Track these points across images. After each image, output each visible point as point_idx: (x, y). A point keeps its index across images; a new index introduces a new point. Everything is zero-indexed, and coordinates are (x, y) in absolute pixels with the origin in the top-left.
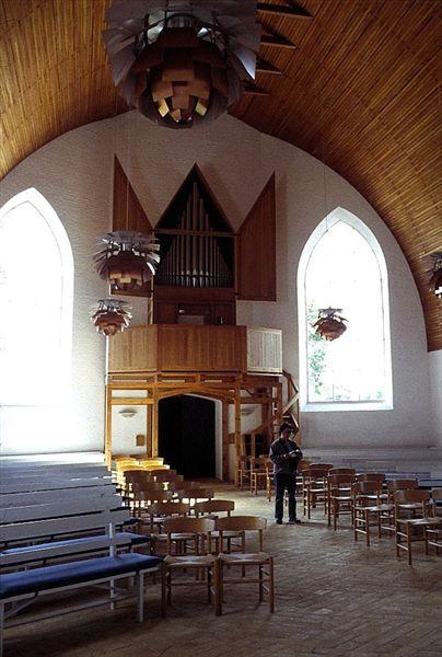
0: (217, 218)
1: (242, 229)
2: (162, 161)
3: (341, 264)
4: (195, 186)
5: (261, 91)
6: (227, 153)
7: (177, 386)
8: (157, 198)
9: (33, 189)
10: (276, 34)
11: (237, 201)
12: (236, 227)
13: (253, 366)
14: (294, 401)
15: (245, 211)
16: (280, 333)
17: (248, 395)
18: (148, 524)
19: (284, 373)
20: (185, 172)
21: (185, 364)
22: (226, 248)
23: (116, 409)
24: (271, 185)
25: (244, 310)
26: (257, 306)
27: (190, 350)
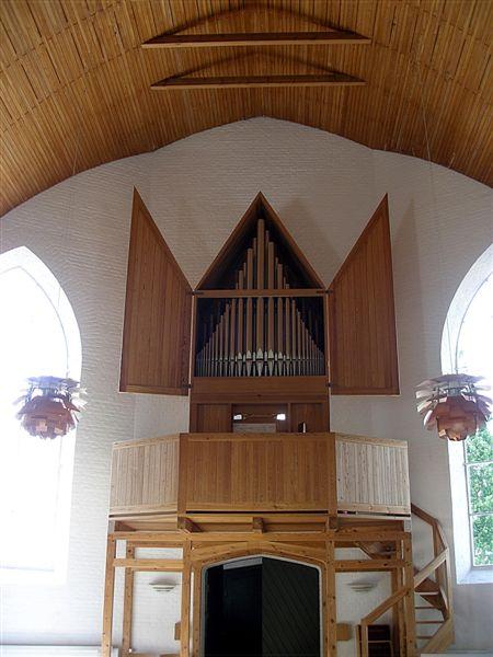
0: (295, 269)
1: (336, 283)
2: (213, 183)
3: (236, 418)
4: (259, 223)
5: (353, 78)
6: (312, 180)
7: (239, 545)
8: (197, 250)
9: (24, 247)
10: (336, 72)
11: (327, 245)
12: (327, 285)
13: (347, 497)
14: (446, 556)
15: (344, 245)
16: (404, 447)
17: (366, 557)
18: (149, 565)
19: (416, 511)
20: (246, 203)
21: (227, 500)
22: (312, 312)
23: (143, 579)
24: (382, 213)
25: (343, 411)
26: (377, 405)
27: (234, 477)
